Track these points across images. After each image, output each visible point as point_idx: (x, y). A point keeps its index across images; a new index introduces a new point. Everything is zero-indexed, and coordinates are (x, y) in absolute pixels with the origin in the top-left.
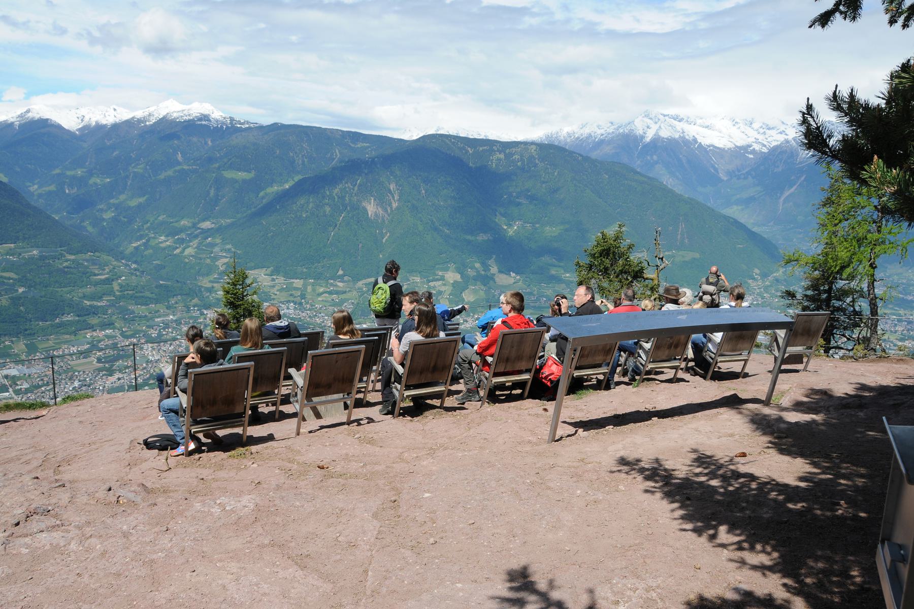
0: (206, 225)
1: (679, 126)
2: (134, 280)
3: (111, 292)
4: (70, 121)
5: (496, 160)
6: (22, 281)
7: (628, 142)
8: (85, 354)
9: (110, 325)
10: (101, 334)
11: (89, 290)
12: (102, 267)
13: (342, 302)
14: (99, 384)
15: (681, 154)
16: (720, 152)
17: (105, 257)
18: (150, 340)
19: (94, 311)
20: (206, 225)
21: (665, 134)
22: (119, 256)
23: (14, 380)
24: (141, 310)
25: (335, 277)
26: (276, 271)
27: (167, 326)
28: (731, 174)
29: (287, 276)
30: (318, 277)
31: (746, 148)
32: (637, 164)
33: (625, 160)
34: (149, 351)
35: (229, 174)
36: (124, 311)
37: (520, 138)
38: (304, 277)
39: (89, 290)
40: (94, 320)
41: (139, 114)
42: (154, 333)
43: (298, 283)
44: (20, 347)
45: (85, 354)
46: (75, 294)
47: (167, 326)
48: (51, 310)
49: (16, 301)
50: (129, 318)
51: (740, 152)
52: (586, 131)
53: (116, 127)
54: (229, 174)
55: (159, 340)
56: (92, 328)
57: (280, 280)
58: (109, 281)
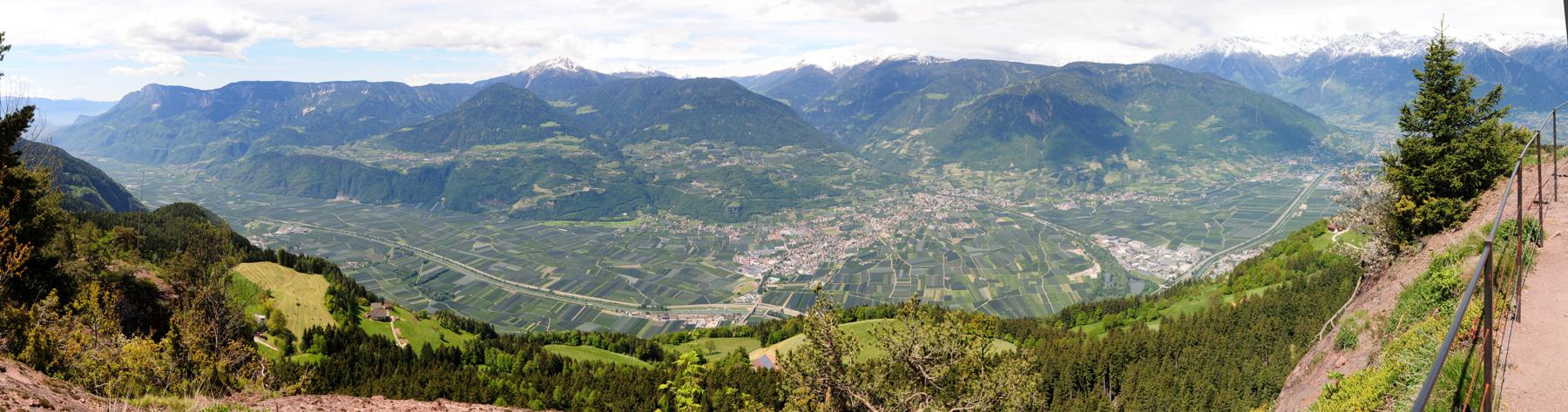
0: (916, 132)
1: (1248, 44)
2: (865, 172)
3: (850, 180)
4: (828, 67)
5: (906, 70)
6: (796, 171)
7: (1212, 58)
8: (832, 223)
9: (848, 203)
10: (843, 209)
11: (836, 178)
12: (845, 161)
13: (1013, 188)
14: (840, 246)
15: (1251, 64)
16: (1277, 59)
17: (847, 155)
18: (875, 215)
19: (838, 193)
20: (916, 132)
21: (1238, 50)
22: (856, 155)
23: (787, 237)
24: (869, 193)
25: (1008, 169)
26: (965, 165)
27: (887, 205)
28: (1286, 73)
29: (973, 168)
30: (995, 169)
31: (1294, 56)
32: (1221, 73)
33: (1212, 70)
34: (875, 224)
35: (931, 96)
36: (858, 194)
37: (1138, 61)
38: (985, 169)
39: (836, 178)
40: (839, 200)
41: (870, 59)
42: (878, 211)
43: (981, 173)
44: (792, 215)
45: (832, 223)
46: (829, 181)
47: (887, 205)
48: (812, 191)
49: (792, 183)
50: (862, 199)
51: (1291, 58)
52: (1183, 53)
53: (855, 67)
54: (931, 96)
55: (881, 216)
56: (837, 205)
57: (968, 171)
58: (849, 172)
